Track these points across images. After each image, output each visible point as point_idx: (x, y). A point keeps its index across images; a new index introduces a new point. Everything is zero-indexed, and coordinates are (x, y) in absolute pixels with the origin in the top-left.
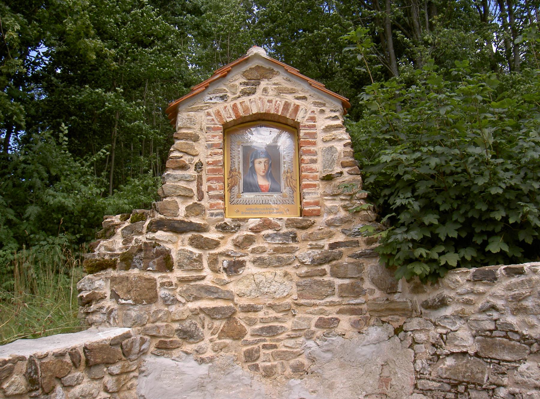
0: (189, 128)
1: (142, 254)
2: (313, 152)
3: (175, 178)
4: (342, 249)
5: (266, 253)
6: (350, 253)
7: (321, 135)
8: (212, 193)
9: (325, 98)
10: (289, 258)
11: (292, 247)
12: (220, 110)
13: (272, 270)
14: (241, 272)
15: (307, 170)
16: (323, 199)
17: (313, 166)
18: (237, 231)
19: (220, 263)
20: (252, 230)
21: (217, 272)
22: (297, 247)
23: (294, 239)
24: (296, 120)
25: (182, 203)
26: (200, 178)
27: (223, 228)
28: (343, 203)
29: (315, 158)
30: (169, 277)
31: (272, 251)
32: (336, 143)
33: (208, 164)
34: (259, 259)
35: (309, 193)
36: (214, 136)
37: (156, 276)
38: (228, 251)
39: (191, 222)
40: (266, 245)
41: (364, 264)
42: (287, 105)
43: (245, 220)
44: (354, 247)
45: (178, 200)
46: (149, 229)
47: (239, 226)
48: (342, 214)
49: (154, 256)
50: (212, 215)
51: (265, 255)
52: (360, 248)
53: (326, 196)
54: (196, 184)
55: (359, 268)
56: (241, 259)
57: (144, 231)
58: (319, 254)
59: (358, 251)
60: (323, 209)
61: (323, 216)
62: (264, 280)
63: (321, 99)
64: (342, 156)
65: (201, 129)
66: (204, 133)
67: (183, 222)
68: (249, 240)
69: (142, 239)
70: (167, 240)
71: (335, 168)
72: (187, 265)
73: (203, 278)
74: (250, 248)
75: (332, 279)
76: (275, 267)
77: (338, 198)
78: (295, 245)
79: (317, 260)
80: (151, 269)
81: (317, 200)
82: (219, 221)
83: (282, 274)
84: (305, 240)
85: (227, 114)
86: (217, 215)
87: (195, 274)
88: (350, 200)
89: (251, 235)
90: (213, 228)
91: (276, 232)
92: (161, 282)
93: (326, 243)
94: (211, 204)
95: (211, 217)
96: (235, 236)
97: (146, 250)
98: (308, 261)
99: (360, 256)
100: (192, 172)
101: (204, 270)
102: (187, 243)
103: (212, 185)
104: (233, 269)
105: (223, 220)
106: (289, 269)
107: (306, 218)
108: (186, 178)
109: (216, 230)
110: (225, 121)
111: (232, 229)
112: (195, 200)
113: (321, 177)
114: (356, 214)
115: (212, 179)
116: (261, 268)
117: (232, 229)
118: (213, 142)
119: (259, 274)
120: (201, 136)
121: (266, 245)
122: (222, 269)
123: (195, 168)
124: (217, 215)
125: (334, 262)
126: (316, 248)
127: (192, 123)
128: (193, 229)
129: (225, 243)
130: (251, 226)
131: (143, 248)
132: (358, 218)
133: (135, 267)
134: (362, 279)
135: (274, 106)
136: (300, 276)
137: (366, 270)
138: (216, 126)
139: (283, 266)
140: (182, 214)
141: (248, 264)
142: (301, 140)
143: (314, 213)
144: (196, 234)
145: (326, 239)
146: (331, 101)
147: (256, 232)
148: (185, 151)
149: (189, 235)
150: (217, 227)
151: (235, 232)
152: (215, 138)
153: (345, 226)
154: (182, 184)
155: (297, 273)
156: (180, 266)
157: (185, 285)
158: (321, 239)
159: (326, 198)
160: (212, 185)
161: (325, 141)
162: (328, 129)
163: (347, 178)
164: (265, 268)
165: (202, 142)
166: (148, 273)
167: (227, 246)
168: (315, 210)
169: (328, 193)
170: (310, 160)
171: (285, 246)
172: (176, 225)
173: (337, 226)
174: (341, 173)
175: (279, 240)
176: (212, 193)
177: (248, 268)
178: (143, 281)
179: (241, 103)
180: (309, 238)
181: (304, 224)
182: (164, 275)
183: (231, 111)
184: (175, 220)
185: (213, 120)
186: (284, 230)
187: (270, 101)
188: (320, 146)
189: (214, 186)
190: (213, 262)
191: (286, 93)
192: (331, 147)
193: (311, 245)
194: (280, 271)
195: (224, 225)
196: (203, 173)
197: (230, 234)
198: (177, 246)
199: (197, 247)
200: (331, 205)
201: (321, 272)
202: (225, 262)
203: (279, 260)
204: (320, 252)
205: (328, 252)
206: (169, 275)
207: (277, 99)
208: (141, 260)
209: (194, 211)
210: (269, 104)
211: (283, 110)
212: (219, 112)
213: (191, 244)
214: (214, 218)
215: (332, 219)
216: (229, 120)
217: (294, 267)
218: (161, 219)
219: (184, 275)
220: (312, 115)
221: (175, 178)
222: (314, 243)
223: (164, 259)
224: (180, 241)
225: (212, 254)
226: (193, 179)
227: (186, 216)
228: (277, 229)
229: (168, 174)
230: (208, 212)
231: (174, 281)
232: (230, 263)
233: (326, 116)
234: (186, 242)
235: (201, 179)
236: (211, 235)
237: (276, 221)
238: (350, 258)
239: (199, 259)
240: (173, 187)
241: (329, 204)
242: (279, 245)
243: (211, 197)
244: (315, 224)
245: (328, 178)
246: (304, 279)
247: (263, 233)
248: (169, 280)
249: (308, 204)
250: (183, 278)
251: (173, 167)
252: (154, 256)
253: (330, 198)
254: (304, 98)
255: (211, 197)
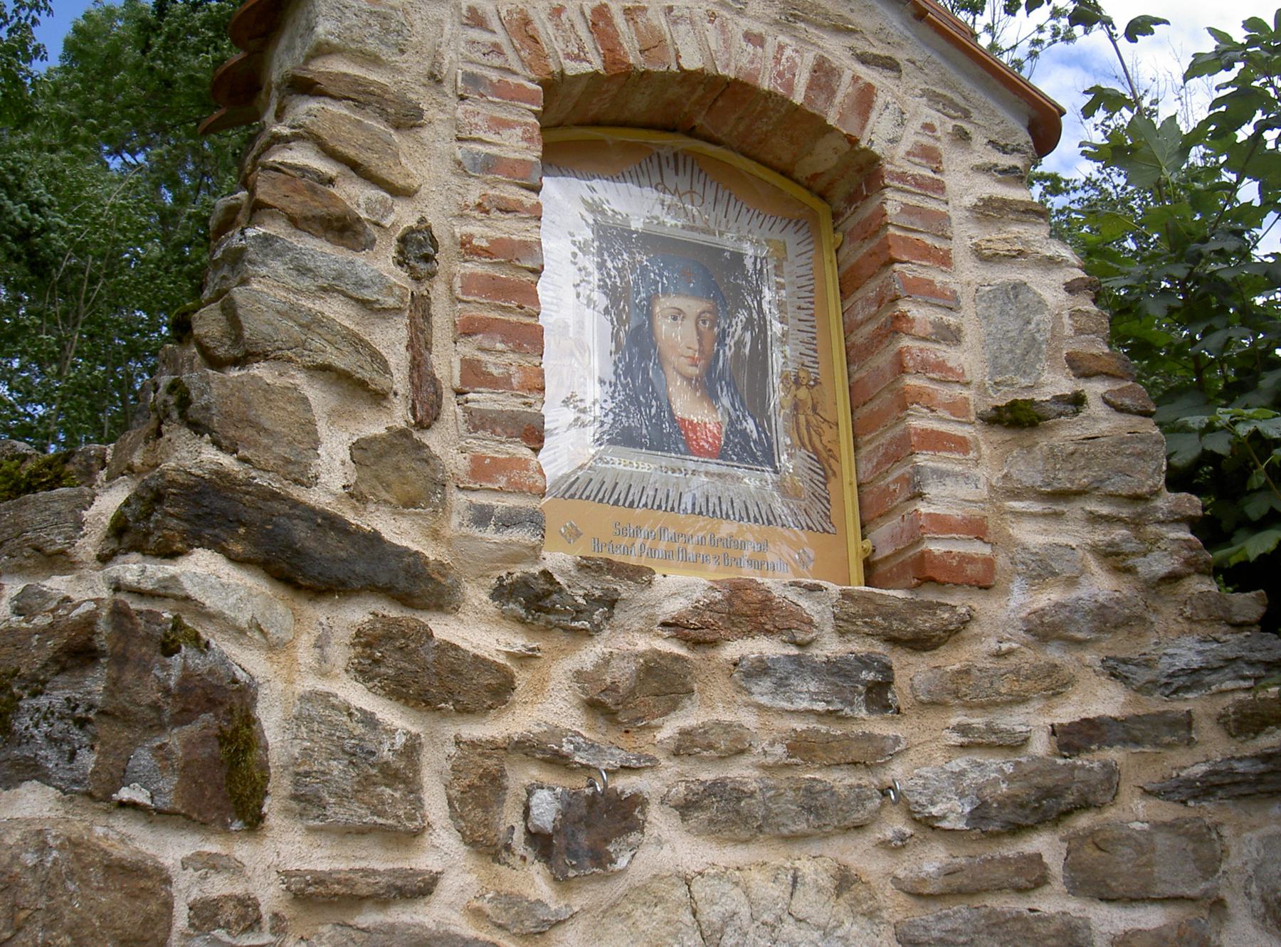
0: (373, 60)
1: (95, 684)
2: (942, 295)
3: (302, 271)
4: (1114, 755)
5: (746, 760)
6: (1151, 775)
7: (965, 235)
8: (483, 399)
9: (967, 86)
10: (860, 797)
11: (869, 737)
12: (531, 13)
13: (776, 856)
14: (622, 862)
15: (925, 367)
16: (1001, 512)
17: (952, 356)
18: (598, 628)
19: (510, 799)
20: (674, 627)
21: (496, 858)
22: (897, 740)
23: (879, 696)
24: (863, 144)
25: (334, 416)
26: (421, 307)
27: (532, 600)
28: (1100, 536)
29: (951, 319)
30: (236, 869)
31: (780, 750)
32: (1030, 273)
33: (467, 248)
34: (716, 789)
35: (941, 475)
36: (499, 125)
37: (171, 849)
38: (556, 733)
39: (375, 538)
40: (749, 719)
41: (1226, 831)
42: (824, 75)
43: (639, 575)
44: (1169, 746)
45: (317, 395)
46: (126, 535)
47: (610, 602)
48: (1101, 585)
49: (168, 711)
50: (482, 516)
51: (742, 772)
52: (1198, 752)
53: (1016, 495)
54: (404, 334)
55: (1205, 850)
56: (625, 784)
57: (88, 546)
58: (1009, 779)
59: (1193, 764)
60: (1001, 561)
61: (1007, 592)
62: (745, 911)
63: (953, 88)
64: (1068, 331)
65: (435, 79)
66: (452, 102)
67: (332, 523)
68: (663, 683)
69: (82, 590)
70: (243, 619)
71: (1046, 377)
72: (342, 796)
73: (420, 888)
74: (669, 729)
75: (1073, 906)
76: (792, 838)
77: (1074, 509)
78: (880, 727)
79: (1002, 805)
80: (142, 797)
81: (975, 511)
82: (517, 558)
83: (826, 882)
84: (935, 704)
85: (567, 42)
86: (509, 521)
87: (379, 861)
88: (1135, 524)
89: (677, 658)
90: (476, 595)
91: (794, 651)
92: (195, 894)
93: (1035, 723)
94: (477, 461)
95: (475, 532)
96: (589, 655)
97: (120, 660)
98: (953, 810)
99: (1206, 788)
100: (380, 264)
101: (428, 839)
102: (341, 663)
103: (483, 357)
104: (583, 839)
105: (534, 553)
106: (858, 854)
107: (930, 596)
108: (360, 284)
109: (491, 607)
110: (554, 67)
111: (579, 613)
112: (399, 415)
113: (986, 406)
114: (1164, 589)
115: (486, 327)
116: (722, 842)
117: (579, 613)
118: (494, 150)
119: (718, 876)
120: (430, 113)
121: (749, 719)
122: (519, 837)
123: (401, 252)
124: (509, 521)
125: (1083, 821)
126: (990, 746)
127: (392, 38)
128: (383, 579)
129: (539, 689)
130: (673, 608)
131: (102, 642)
132: (1170, 611)
133: (32, 770)
134: (1218, 906)
135: (770, 63)
136: (917, 893)
137: (1233, 862)
138: (511, 79)
139: (827, 836)
140: (330, 478)
141: (659, 820)
142: (891, 230)
143: (970, 570)
144: (394, 612)
145: (1036, 705)
146: (991, 103)
147: (696, 644)
148: (351, 152)
149: (358, 614)
150: (502, 593)
151: (587, 634)
152: (506, 133)
153: (1119, 645)
154: (337, 311)
155: (901, 873)
156: (306, 802)
157: (326, 930)
158: (1010, 703)
159: (1018, 505)
160: (483, 357)
161: (984, 257)
162: (989, 211)
163: (1103, 427)
164: (738, 841)
165: (437, 134)
166: (122, 825)
167: (547, 706)
168: (971, 560)
169: (1029, 483)
170: (934, 324)
171: (837, 730)
172: (302, 533)
173: (1080, 643)
174: (1077, 401)
175: (814, 697)
176: (483, 399)
177: (659, 842)
178: (95, 875)
179: (627, 11)
180: (956, 694)
181: (924, 623)
182: (213, 846)
183: (583, 31)
184: (296, 504)
185: (496, 49)
186: (830, 647)
187: (755, 39)
188: (966, 276)
189: (494, 366)
190: (479, 789)
191: (819, 26)
192: (1018, 287)
193: (963, 729)
194: (814, 864)
195: (542, 585)
196: (438, 289)
197: (560, 639)
198: (296, 668)
199: (399, 691)
200: (1041, 539)
201: (1019, 872)
202: (542, 797)
203: (815, 804)
204: (1008, 768)
205: (1055, 769)
206: (242, 851)
207: (782, 39)
208: (82, 723)
209: (392, 477)
210: (750, 48)
211: (809, 88)
212: (527, 22)
213: (365, 672)
214: (490, 535)
215: (1060, 606)
216: (572, 68)
217: (884, 845)
218: (221, 474)
219: (323, 859)
220: (925, 140)
221: (302, 271)
222: (978, 721)
223: (223, 739)
224: (306, 640)
225: (473, 744)
226: (391, 302)
227: (355, 495)
228: (800, 637)
229: (267, 240)
230: (459, 499)
231: (270, 896)
232: (569, 802)
233: (978, 162)
234: (340, 654)
235: (427, 316)
236: (467, 633)
237: (792, 595)
238: (1153, 802)
239: (402, 772)
240: (290, 312)
241: (1032, 535)
242: (813, 724)
243: (479, 422)
244: (974, 629)
245: (1017, 418)
246: (936, 908)
247: (735, 649)
248: (239, 890)
249: (942, 525)
250: (320, 879)
251: (295, 209)
252: (168, 711)
253: (1037, 507)
254: (889, 65)
255: (479, 422)
